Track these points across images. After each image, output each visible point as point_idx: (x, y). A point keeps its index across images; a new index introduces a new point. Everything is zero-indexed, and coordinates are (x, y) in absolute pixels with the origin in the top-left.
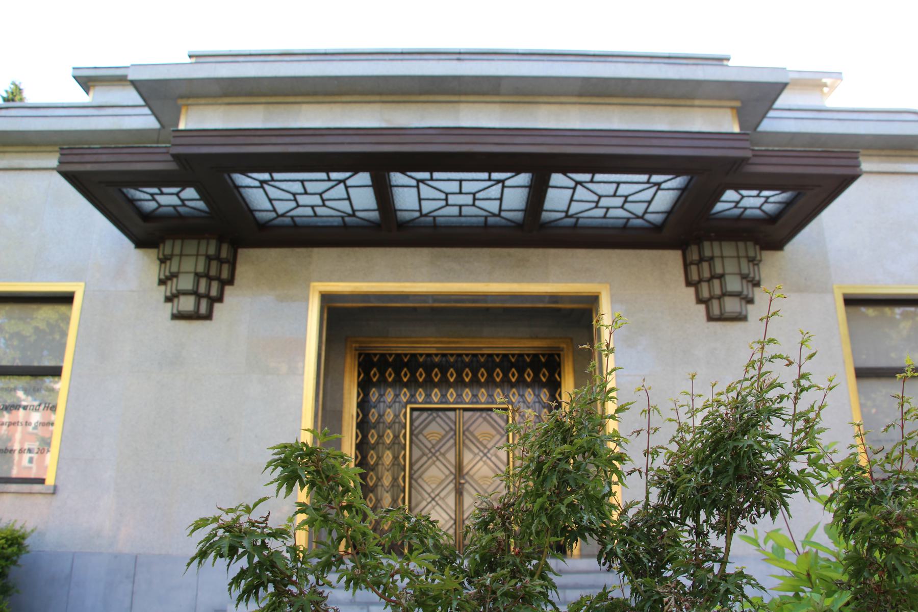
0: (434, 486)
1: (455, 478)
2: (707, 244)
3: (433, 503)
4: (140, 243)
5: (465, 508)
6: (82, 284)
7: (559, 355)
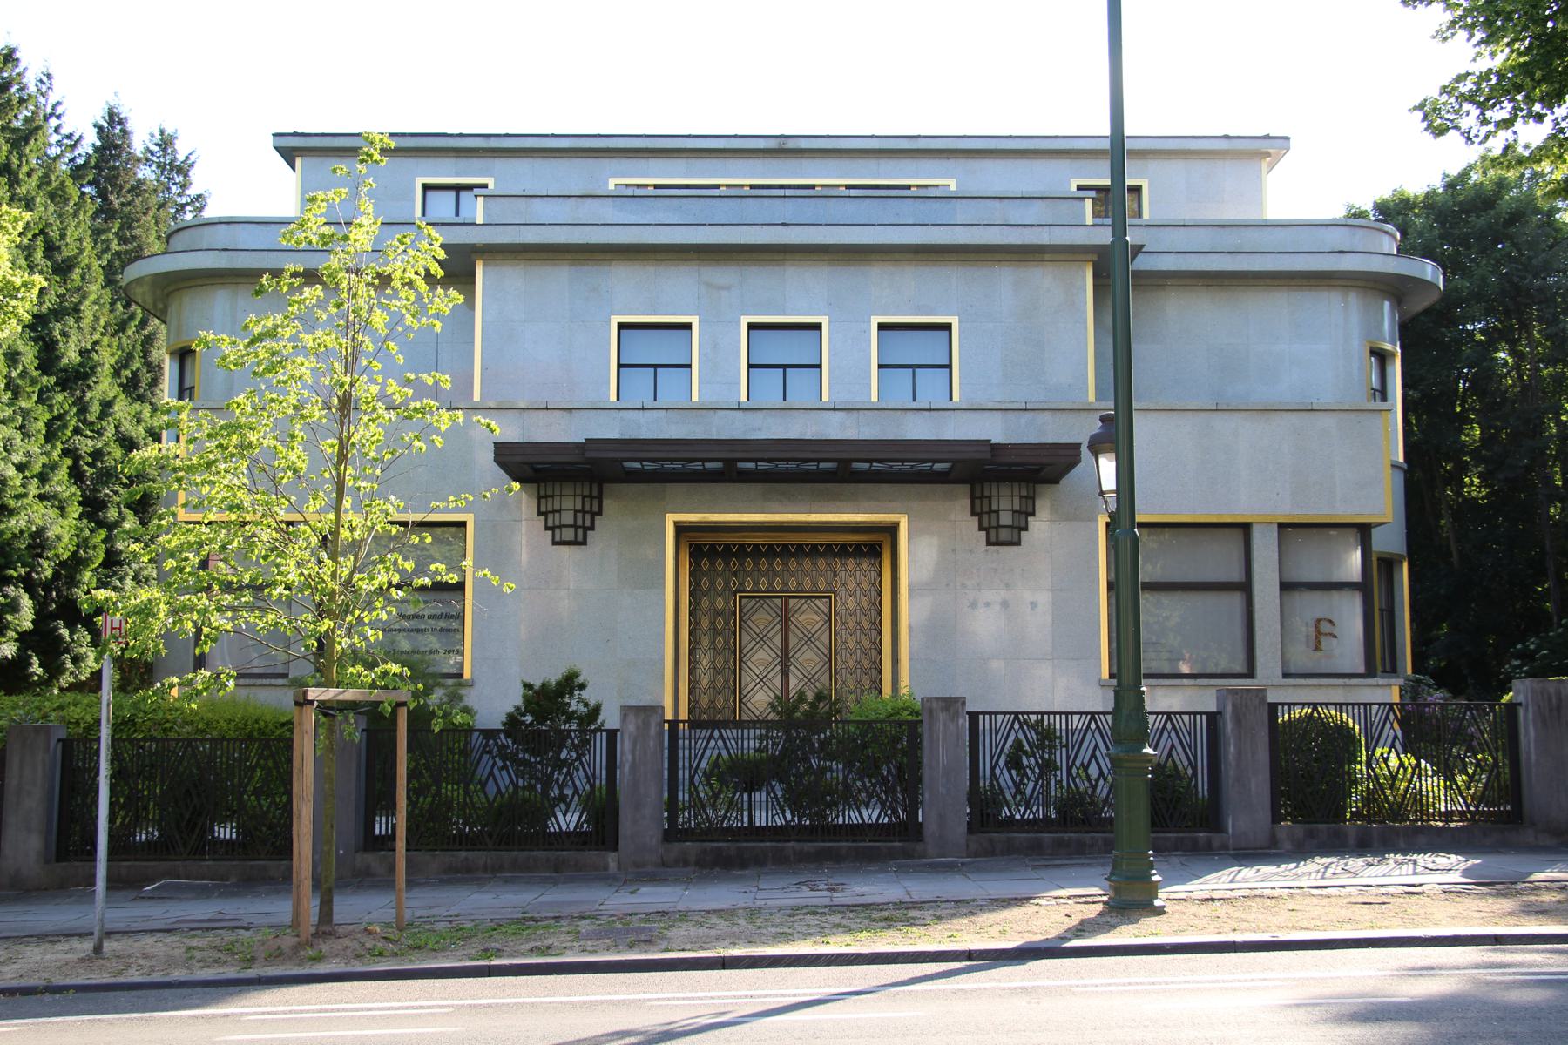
0: (761, 668)
2: (986, 485)
5: (780, 634)
7: (880, 546)
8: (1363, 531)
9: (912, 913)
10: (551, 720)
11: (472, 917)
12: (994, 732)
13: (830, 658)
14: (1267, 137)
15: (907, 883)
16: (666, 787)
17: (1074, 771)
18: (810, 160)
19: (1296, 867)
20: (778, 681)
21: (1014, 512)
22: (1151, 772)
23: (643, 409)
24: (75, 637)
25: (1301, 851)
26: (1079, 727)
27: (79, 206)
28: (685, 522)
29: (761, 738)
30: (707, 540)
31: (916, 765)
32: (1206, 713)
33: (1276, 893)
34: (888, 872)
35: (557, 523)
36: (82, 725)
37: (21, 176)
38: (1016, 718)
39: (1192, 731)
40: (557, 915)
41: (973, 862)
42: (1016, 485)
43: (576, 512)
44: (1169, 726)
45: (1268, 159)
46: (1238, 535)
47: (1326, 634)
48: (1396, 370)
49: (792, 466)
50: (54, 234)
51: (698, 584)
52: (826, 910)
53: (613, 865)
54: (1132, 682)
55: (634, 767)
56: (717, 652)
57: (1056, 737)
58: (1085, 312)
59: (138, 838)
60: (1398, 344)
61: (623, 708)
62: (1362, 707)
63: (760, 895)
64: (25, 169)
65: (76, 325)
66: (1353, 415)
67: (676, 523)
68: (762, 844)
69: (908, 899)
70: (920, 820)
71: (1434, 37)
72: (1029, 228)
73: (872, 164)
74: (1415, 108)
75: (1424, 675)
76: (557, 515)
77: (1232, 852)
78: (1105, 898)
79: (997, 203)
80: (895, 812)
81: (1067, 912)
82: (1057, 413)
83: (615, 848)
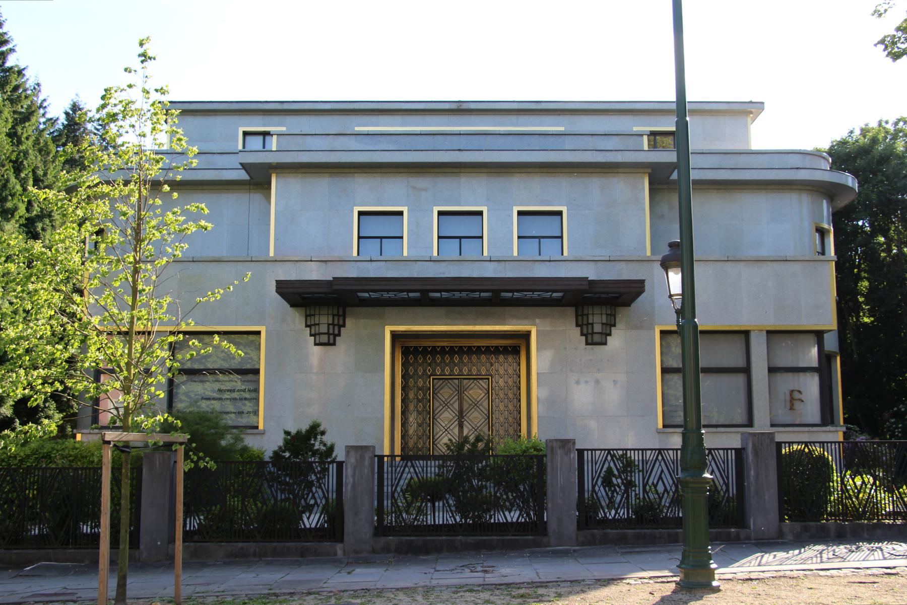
0: (446, 423)
1: (459, 418)
3: (446, 432)
4: (293, 305)
6: (264, 327)
7: (519, 347)
8: (819, 335)
9: (541, 591)
10: (302, 455)
11: (234, 593)
12: (594, 462)
13: (489, 417)
14: (751, 102)
15: (537, 566)
16: (376, 498)
17: (648, 487)
18: (476, 116)
19: (800, 553)
20: (456, 431)
21: (603, 324)
22: (709, 491)
23: (371, 261)
24: (47, 405)
25: (800, 541)
26: (651, 459)
27: (55, 157)
28: (399, 331)
29: (439, 467)
30: (413, 343)
31: (543, 484)
32: (735, 449)
33: (795, 574)
34: (524, 557)
35: (317, 332)
36: (18, 458)
37: (23, 139)
38: (609, 453)
39: (726, 461)
40: (292, 591)
41: (581, 550)
42: (604, 308)
43: (329, 325)
44: (660, 458)
45: (751, 115)
46: (741, 339)
47: (797, 400)
48: (831, 240)
49: (464, 294)
50: (40, 172)
51: (407, 371)
52: (480, 588)
53: (340, 552)
54: (695, 426)
55: (354, 486)
56: (419, 413)
57: (635, 466)
58: (644, 204)
59: (33, 532)
60: (832, 225)
61: (347, 447)
62: (837, 444)
63: (437, 575)
64: (25, 135)
65: (50, 224)
66: (812, 263)
67: (392, 332)
68: (440, 538)
69: (538, 580)
70: (545, 520)
71: (873, 15)
72: (610, 152)
73: (513, 118)
74: (879, 43)
75: (853, 425)
76: (317, 327)
77: (753, 541)
78: (677, 579)
79: (590, 138)
80: (528, 515)
81: (650, 590)
82: (629, 262)
83: (342, 541)
